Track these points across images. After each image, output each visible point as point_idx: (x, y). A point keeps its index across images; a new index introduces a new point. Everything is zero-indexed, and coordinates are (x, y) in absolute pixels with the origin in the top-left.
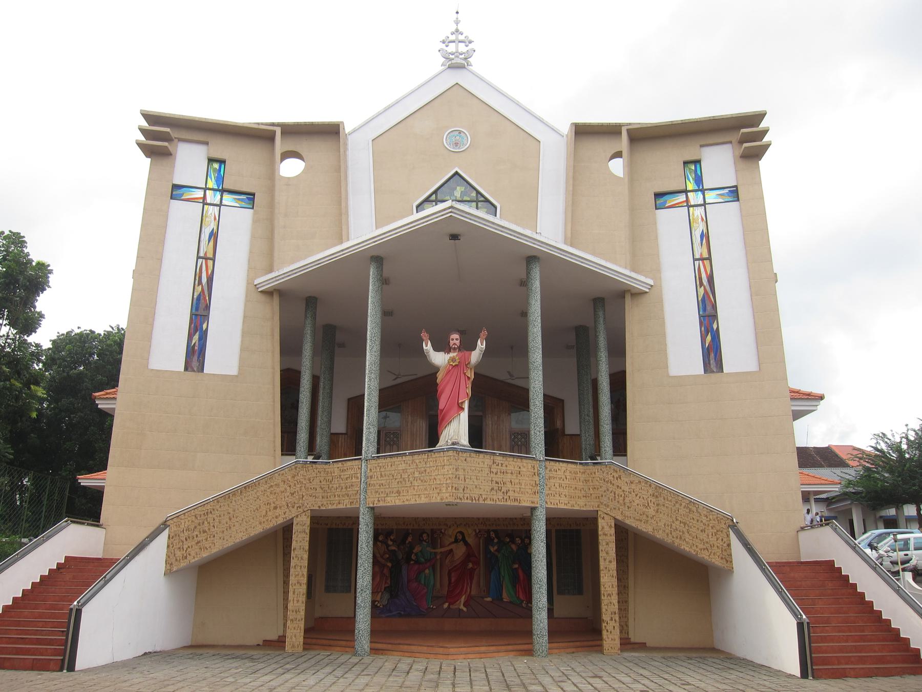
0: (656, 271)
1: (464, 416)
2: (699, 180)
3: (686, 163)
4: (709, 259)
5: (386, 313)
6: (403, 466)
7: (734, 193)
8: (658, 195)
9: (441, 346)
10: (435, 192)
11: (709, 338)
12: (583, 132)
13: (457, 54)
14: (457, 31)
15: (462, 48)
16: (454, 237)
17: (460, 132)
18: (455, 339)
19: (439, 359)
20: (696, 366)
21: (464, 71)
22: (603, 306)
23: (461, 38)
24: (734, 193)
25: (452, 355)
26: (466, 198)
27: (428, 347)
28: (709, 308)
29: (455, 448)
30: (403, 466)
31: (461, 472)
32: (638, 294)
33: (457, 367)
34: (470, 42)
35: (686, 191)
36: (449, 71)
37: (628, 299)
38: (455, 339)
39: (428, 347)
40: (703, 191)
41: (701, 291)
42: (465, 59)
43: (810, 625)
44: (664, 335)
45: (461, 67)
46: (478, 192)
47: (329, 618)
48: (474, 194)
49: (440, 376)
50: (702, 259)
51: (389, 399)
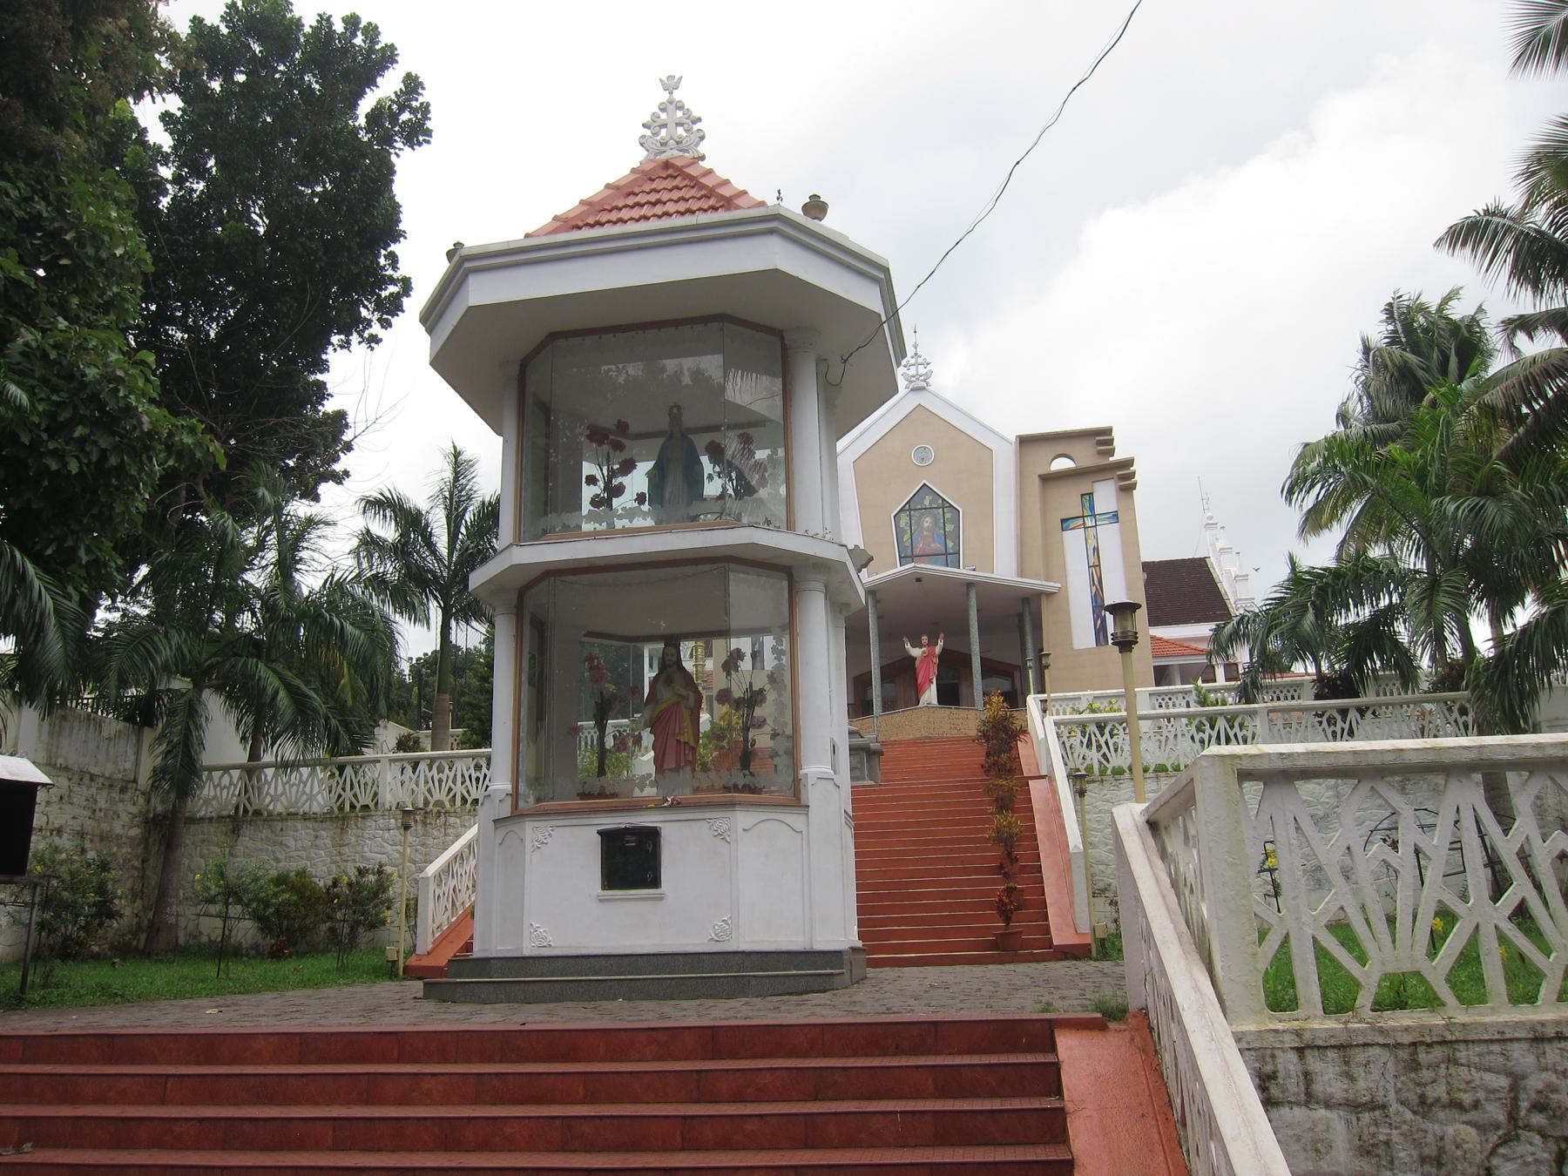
0: (1063, 578)
1: (934, 687)
2: (1092, 507)
3: (1082, 495)
4: (1099, 565)
5: (879, 618)
6: (898, 719)
7: (1115, 516)
8: (1063, 521)
9: (917, 643)
10: (908, 502)
11: (1099, 622)
12: (1025, 441)
13: (917, 376)
14: (916, 354)
15: (922, 370)
16: (919, 580)
17: (925, 448)
18: (925, 639)
19: (916, 652)
20: (1090, 641)
21: (925, 393)
22: (1029, 603)
23: (920, 360)
24: (1115, 516)
25: (924, 649)
26: (934, 506)
27: (908, 646)
28: (1099, 601)
29: (929, 707)
30: (898, 719)
31: (931, 720)
32: (1049, 595)
33: (926, 657)
34: (928, 364)
35: (1083, 517)
36: (912, 394)
37: (1044, 600)
38: (925, 639)
39: (908, 646)
40: (1094, 516)
41: (1094, 589)
42: (925, 380)
43: (769, 642)
44: (1069, 622)
45: (922, 389)
46: (943, 500)
47: (940, 398)
48: (940, 501)
49: (917, 663)
50: (1094, 566)
51: (888, 674)
